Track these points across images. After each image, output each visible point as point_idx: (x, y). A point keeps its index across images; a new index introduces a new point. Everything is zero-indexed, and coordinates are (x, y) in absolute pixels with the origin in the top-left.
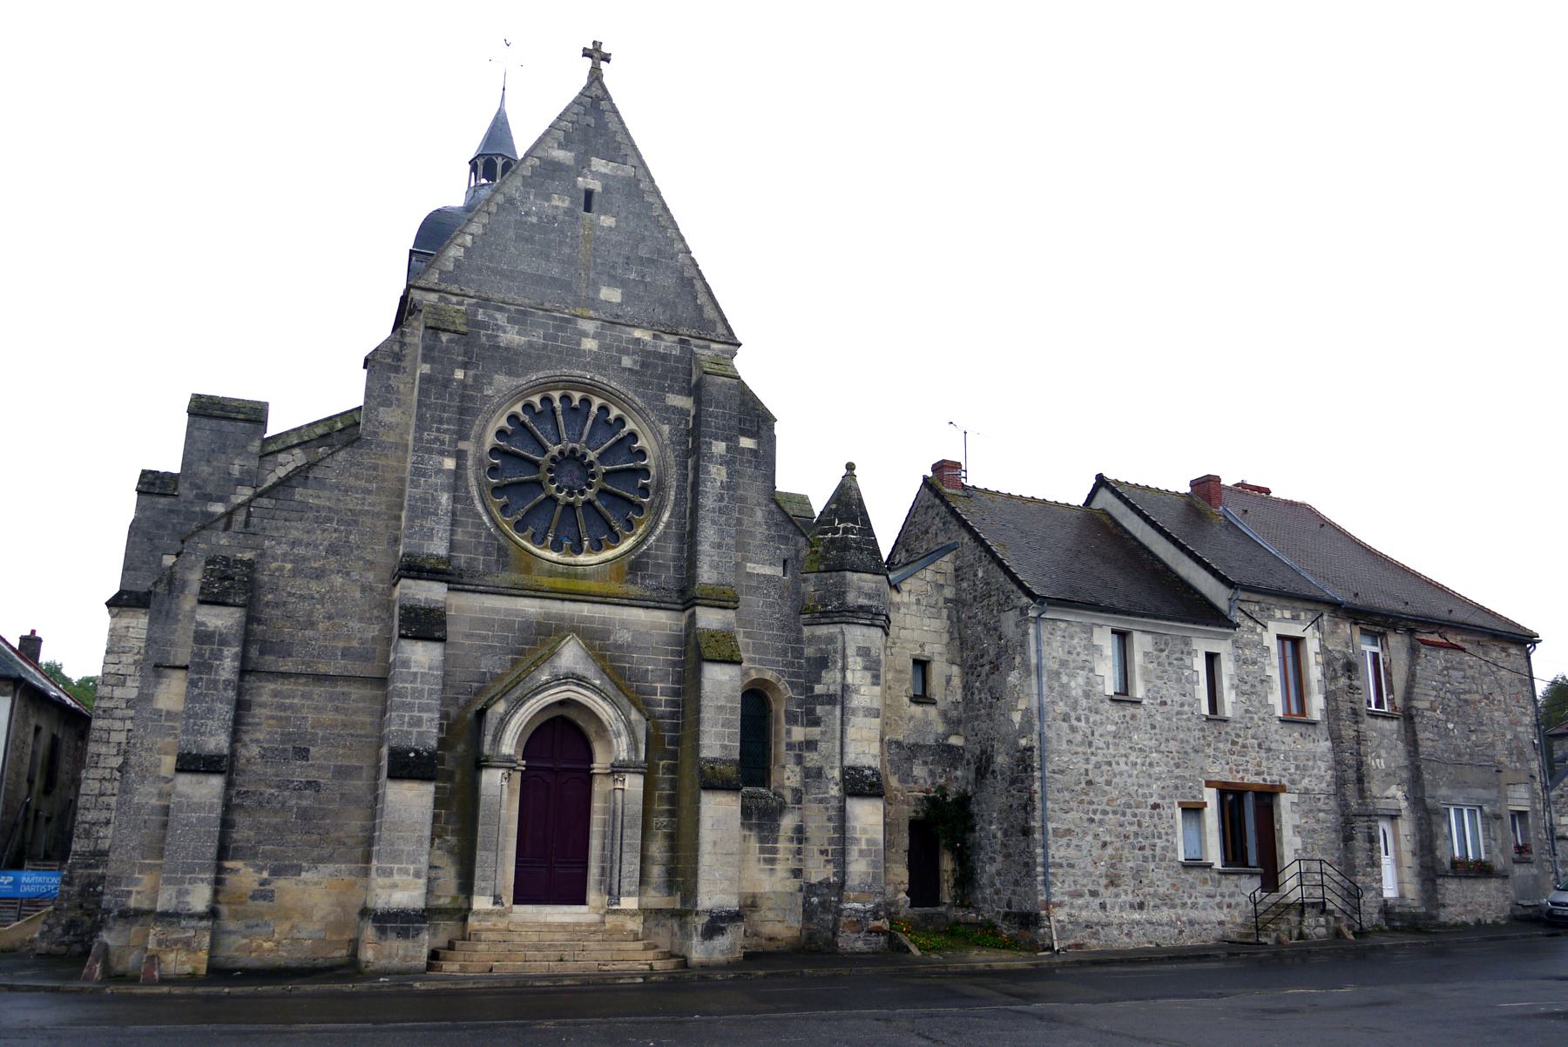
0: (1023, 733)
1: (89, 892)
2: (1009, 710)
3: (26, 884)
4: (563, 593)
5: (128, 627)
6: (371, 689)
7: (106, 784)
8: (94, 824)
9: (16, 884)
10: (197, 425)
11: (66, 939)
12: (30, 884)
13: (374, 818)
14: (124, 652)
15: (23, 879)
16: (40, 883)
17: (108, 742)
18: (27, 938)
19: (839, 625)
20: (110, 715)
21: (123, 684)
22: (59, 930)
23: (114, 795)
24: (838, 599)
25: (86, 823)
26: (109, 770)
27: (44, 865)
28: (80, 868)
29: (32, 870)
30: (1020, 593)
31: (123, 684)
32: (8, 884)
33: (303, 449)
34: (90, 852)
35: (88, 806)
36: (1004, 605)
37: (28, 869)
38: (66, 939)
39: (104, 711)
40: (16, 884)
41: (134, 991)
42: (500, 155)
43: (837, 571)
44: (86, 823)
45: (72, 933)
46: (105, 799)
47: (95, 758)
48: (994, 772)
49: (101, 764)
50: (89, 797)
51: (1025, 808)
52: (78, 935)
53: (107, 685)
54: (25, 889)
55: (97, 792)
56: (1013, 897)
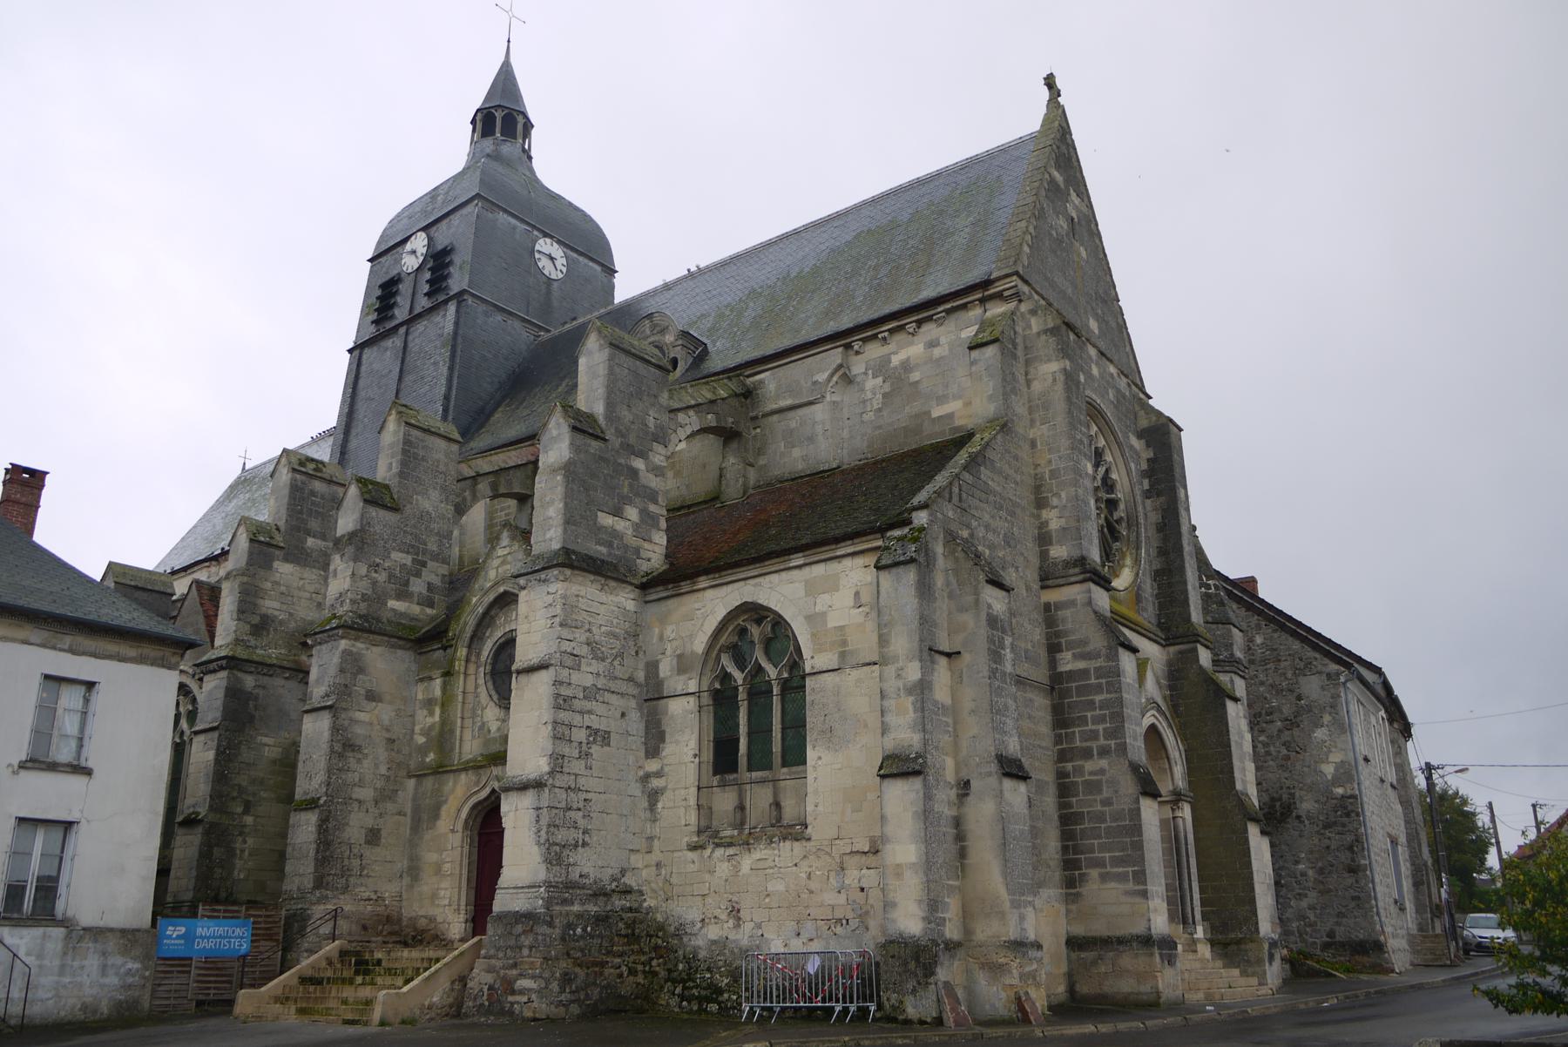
0: (1337, 781)
1: (570, 935)
2: (1316, 762)
3: (202, 938)
4: (1122, 617)
5: (577, 596)
6: (1165, 698)
7: (572, 794)
8: (564, 846)
9: (189, 937)
10: (617, 361)
11: (563, 997)
12: (208, 938)
13: (1034, 847)
14: (576, 628)
15: (199, 930)
16: (220, 937)
17: (570, 741)
18: (427, 1003)
19: (1229, 675)
20: (570, 706)
21: (578, 668)
22: (555, 986)
23: (579, 809)
24: (1226, 650)
25: (557, 844)
26: (573, 777)
27: (225, 911)
28: (557, 904)
29: (209, 917)
30: (1326, 661)
31: (578, 668)
32: (178, 937)
33: (696, 413)
34: (562, 883)
35: (557, 822)
36: (1306, 668)
37: (203, 916)
38: (563, 997)
39: (565, 700)
40: (189, 937)
41: (1064, 1032)
42: (499, 106)
43: (1223, 624)
44: (557, 844)
45: (567, 990)
46: (572, 814)
47: (560, 761)
48: (1298, 817)
49: (566, 770)
50: (557, 811)
51: (1350, 848)
52: (574, 992)
53: (564, 667)
54: (201, 946)
55: (563, 805)
56: (1337, 928)
